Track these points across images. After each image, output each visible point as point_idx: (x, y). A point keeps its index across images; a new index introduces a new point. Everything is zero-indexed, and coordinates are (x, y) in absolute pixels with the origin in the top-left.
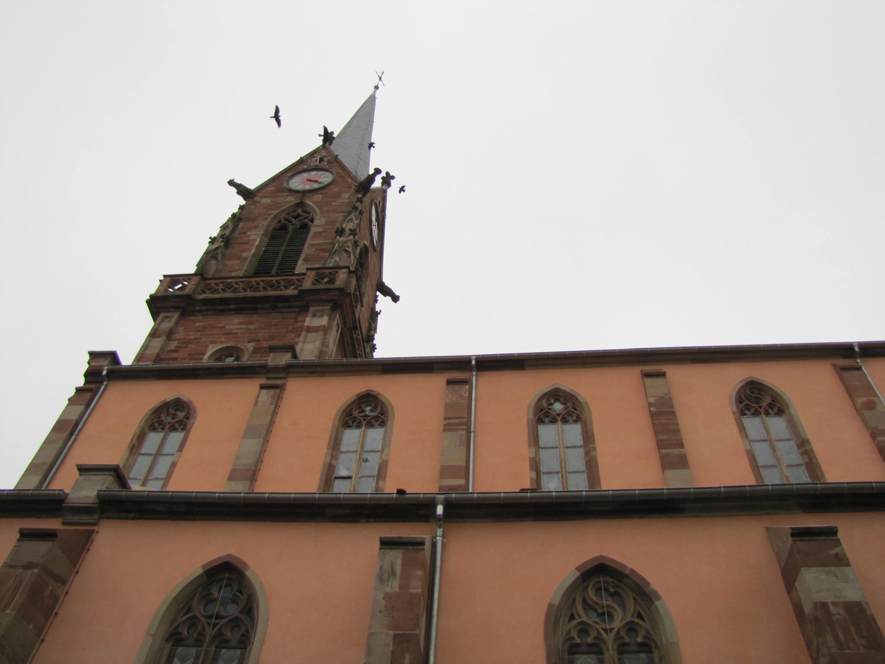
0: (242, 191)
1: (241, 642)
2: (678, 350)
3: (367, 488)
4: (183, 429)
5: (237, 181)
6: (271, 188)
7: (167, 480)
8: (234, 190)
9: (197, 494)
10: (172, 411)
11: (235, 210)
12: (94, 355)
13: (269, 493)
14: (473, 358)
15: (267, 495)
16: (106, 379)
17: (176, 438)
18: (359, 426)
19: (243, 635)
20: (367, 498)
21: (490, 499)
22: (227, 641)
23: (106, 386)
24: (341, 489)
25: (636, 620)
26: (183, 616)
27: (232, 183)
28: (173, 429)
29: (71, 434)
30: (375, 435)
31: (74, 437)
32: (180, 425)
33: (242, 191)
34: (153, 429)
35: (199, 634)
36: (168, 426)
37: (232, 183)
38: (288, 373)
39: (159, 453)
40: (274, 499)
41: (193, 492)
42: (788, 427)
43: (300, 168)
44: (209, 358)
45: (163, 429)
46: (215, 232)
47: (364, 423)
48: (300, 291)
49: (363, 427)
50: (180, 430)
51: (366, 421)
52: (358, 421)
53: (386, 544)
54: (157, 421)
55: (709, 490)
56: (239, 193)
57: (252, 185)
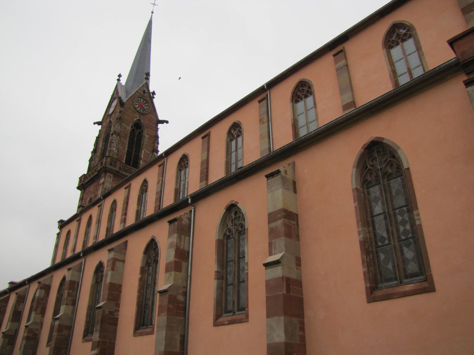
0: (99, 123)
1: (377, 180)
2: (284, 72)
3: (313, 128)
4: (311, 94)
5: (96, 121)
6: (106, 117)
7: (317, 119)
8: (96, 125)
9: (219, 181)
10: (301, 89)
11: (97, 134)
12: (59, 222)
13: (313, 131)
14: (265, 85)
15: (368, 104)
16: (268, 90)
17: (310, 100)
18: (398, 44)
19: (397, 168)
20: (344, 117)
21: (340, 120)
22: (370, 182)
23: (270, 92)
24: (303, 133)
25: (392, 159)
26: (365, 170)
27: (95, 123)
28: (306, 96)
29: (268, 121)
30: (409, 45)
31: (270, 122)
32: (308, 93)
33: (99, 123)
34: (297, 101)
35: (376, 177)
36: (303, 97)
37: (95, 123)
38: (82, 214)
39: (307, 110)
40: (348, 116)
41: (278, 150)
42: (297, 109)
43: (112, 100)
44: (88, 203)
45: (302, 99)
46: (92, 150)
47: (399, 41)
48: (98, 172)
49: (400, 43)
50: (310, 96)
51: (400, 39)
52: (396, 41)
53: (268, 177)
54: (297, 97)
55: (132, 225)
56: (99, 125)
57: (100, 120)
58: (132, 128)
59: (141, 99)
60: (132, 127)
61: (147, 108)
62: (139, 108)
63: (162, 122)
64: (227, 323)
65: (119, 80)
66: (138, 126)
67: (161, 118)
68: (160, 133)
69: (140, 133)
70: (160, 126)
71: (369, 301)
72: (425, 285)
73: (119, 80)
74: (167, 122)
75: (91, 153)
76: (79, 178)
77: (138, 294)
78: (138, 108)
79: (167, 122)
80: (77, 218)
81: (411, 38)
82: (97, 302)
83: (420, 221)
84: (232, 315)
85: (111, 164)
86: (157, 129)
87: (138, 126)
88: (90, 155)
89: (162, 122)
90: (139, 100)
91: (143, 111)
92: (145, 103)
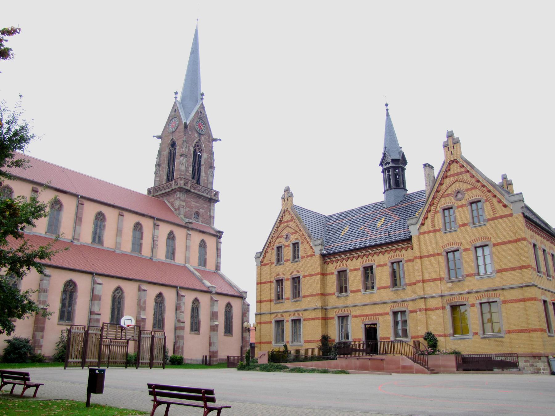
57: (160, 134)
61: (204, 129)
62: (198, 129)
63: (215, 140)
64: (187, 255)
65: (176, 98)
66: (198, 145)
67: (215, 137)
68: (214, 150)
70: (214, 143)
71: (224, 336)
72: (198, 333)
73: (176, 98)
74: (220, 140)
78: (197, 128)
79: (220, 140)
82: (369, 271)
84: (447, 302)
85: (185, 185)
86: (212, 147)
87: (198, 145)
88: (154, 169)
89: (215, 140)
91: (201, 132)
92: (203, 124)
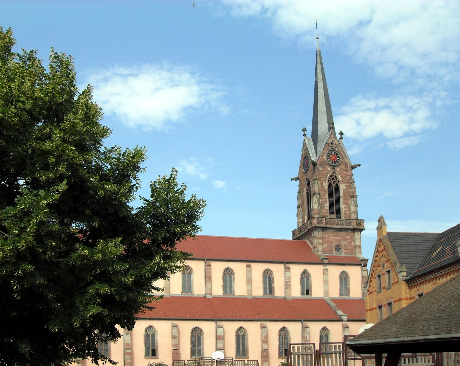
0: (297, 179)
11: (297, 189)
27: (292, 180)
33: (297, 179)
37: (292, 180)
57: (296, 175)
58: (329, 183)
59: (317, 185)
60: (328, 182)
68: (355, 178)
69: (337, 184)
74: (359, 165)
75: (297, 208)
76: (292, 232)
77: (157, 344)
80: (345, 299)
81: (293, 297)
83: (268, 346)
85: (318, 223)
90: (330, 153)
